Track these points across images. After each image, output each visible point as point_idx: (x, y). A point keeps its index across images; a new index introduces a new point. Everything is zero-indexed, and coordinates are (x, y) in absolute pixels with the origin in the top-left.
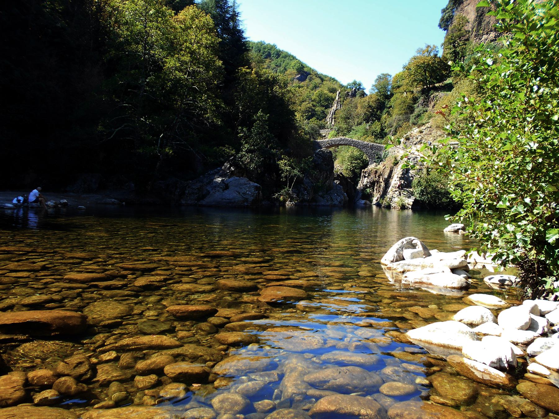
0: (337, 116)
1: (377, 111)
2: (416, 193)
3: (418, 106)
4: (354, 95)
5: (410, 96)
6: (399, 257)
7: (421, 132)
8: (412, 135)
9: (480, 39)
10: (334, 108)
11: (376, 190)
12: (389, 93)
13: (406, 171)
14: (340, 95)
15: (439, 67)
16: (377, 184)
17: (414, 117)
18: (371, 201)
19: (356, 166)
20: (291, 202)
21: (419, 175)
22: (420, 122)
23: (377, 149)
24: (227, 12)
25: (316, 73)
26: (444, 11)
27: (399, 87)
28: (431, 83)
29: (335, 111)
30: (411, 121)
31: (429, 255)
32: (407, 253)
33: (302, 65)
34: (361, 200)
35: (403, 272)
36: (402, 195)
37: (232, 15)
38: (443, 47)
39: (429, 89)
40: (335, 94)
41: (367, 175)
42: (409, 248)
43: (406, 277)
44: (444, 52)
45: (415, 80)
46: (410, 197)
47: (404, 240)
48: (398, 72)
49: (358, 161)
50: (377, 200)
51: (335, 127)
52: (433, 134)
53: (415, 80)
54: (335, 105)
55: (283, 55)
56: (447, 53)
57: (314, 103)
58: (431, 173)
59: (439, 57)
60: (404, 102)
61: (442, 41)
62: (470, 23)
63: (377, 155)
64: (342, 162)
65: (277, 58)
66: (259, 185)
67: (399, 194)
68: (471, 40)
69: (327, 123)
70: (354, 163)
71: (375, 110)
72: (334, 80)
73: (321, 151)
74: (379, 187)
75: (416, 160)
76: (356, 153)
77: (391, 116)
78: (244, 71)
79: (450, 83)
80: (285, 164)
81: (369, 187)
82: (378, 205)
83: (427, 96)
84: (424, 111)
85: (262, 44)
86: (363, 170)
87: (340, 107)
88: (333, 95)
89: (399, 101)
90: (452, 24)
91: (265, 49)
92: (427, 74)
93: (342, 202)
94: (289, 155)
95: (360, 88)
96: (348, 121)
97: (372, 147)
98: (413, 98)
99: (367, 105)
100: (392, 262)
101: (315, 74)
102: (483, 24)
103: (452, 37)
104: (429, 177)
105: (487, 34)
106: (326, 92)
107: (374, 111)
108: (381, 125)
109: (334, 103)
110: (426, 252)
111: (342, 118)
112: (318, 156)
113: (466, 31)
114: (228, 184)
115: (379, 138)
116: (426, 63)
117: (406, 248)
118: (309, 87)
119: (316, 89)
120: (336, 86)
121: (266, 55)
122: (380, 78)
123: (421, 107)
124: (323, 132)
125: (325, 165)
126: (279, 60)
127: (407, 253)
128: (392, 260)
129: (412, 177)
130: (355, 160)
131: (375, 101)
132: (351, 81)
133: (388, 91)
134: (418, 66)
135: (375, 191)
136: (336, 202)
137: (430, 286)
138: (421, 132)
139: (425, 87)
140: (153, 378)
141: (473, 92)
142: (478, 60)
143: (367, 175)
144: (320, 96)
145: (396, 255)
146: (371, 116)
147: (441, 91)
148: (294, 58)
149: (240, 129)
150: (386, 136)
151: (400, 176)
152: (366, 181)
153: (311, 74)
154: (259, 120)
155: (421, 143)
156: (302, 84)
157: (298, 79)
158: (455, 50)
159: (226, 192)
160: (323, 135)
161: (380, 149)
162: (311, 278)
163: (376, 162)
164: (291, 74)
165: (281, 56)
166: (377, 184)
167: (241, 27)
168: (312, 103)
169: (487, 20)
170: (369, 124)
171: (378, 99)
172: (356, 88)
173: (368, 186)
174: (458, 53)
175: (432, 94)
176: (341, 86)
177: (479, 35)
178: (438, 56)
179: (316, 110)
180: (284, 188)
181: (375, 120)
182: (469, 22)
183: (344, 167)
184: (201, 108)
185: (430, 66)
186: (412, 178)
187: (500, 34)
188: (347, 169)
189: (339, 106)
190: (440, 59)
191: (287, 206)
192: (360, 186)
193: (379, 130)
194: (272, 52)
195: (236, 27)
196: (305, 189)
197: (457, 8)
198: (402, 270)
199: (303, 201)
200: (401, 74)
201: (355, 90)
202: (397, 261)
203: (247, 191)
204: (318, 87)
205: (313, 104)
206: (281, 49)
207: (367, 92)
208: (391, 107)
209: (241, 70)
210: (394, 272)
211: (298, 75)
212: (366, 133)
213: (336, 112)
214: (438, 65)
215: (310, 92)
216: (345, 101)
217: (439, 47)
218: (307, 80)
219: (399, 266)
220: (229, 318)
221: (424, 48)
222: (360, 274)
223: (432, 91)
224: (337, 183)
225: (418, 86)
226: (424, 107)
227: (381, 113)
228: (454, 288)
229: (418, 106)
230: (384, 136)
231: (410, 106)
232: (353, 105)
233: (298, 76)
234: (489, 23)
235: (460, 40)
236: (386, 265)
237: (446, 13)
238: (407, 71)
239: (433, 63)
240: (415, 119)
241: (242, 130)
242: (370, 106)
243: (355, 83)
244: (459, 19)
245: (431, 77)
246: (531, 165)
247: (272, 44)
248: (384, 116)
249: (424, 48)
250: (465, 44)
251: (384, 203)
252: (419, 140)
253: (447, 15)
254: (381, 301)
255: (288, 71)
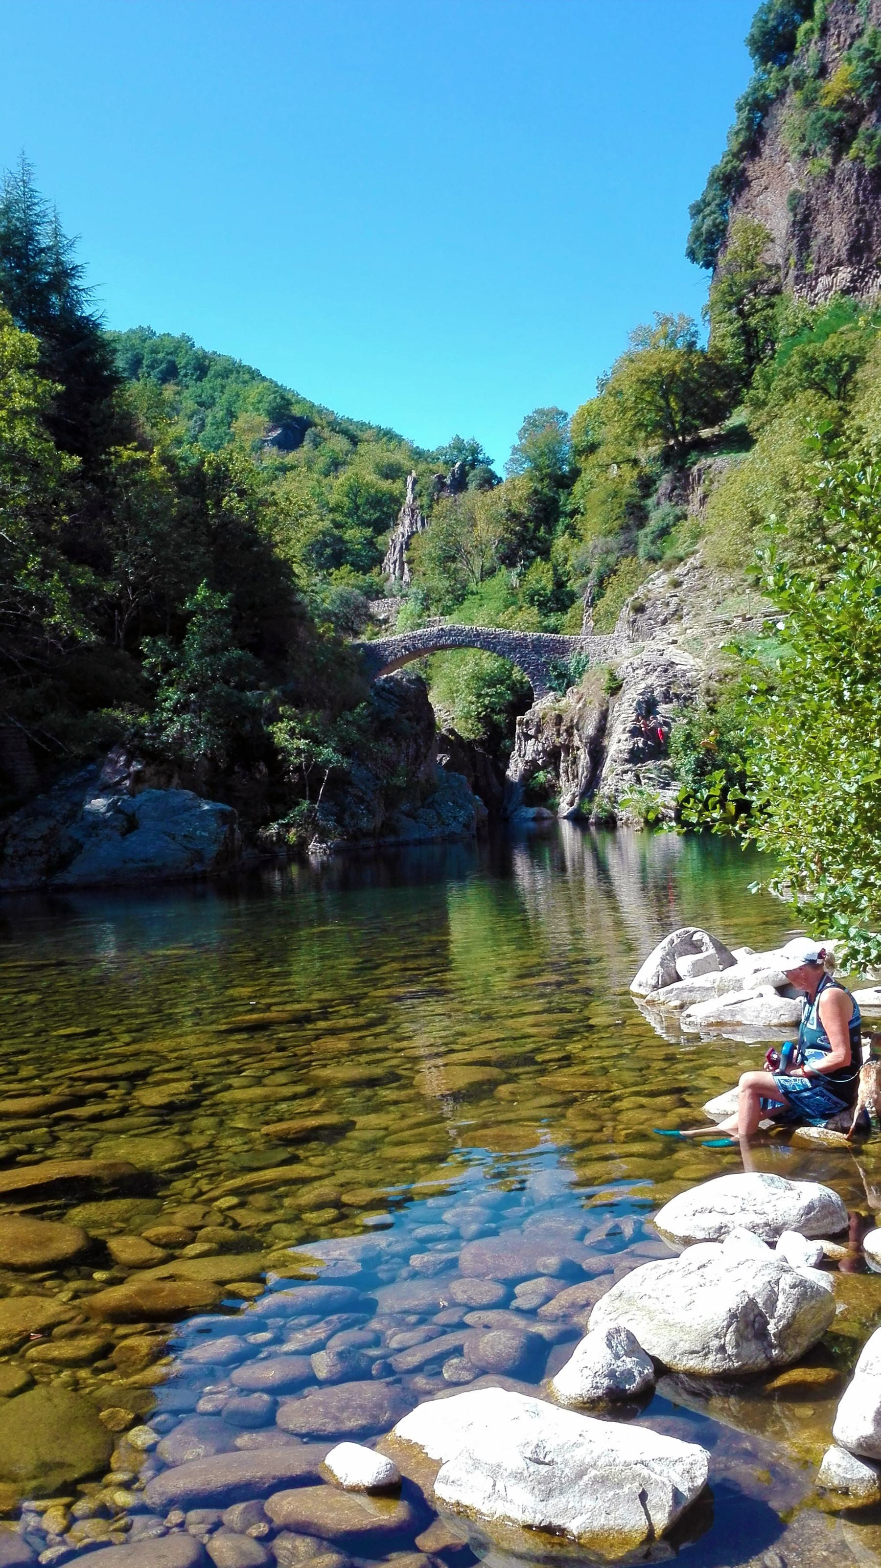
0: (416, 554)
1: (537, 529)
2: (683, 770)
3: (658, 504)
4: (460, 484)
5: (630, 474)
6: (669, 975)
7: (677, 584)
8: (650, 595)
9: (812, 288)
10: (403, 528)
11: (566, 772)
12: (566, 468)
13: (648, 707)
14: (418, 488)
15: (704, 380)
16: (567, 754)
17: (650, 538)
18: (554, 807)
19: (494, 703)
20: (321, 842)
21: (685, 716)
22: (669, 554)
23: (554, 650)
24: (38, 268)
25: (331, 418)
26: (697, 210)
27: (592, 448)
28: (687, 429)
29: (409, 537)
30: (641, 551)
31: (733, 962)
32: (684, 964)
33: (283, 398)
34: (524, 809)
35: (682, 1007)
36: (643, 781)
37: (54, 274)
38: (707, 318)
39: (685, 450)
40: (399, 484)
41: (532, 732)
42: (686, 953)
43: (689, 1016)
44: (714, 330)
45: (640, 426)
46: (669, 785)
47: (673, 935)
48: (584, 403)
49: (501, 688)
50: (571, 804)
51: (414, 589)
52: (711, 587)
53: (640, 426)
54: (407, 522)
55: (218, 368)
56: (724, 336)
57: (339, 518)
58: (719, 707)
59: (702, 351)
60: (615, 494)
61: (704, 298)
62: (778, 241)
63: (555, 668)
64: (452, 695)
65: (199, 379)
66: (228, 808)
67: (634, 779)
68: (787, 291)
69: (387, 579)
70: (487, 695)
71: (531, 525)
72: (388, 436)
73: (392, 678)
74: (575, 762)
75: (670, 674)
76: (490, 663)
77: (581, 540)
78: (129, 457)
79: (742, 427)
80: (292, 733)
81: (544, 767)
82: (579, 819)
83: (681, 469)
84: (678, 518)
85: (145, 334)
86: (518, 718)
87: (423, 525)
88: (395, 487)
89: (597, 494)
90: (726, 247)
91: (154, 351)
92: (673, 404)
93: (474, 825)
94: (297, 701)
95: (475, 460)
96: (453, 566)
97: (538, 646)
98: (640, 477)
99: (503, 511)
100: (656, 987)
101: (329, 424)
102: (816, 244)
103: (730, 285)
104: (716, 719)
105: (829, 272)
106: (371, 477)
107: (526, 528)
108: (555, 570)
109: (401, 514)
110: (724, 956)
111: (432, 559)
112: (384, 694)
113: (769, 267)
114: (134, 815)
115: (551, 610)
116: (665, 373)
117: (681, 955)
118: (316, 467)
119: (336, 469)
120: (399, 457)
121: (161, 372)
122: (532, 424)
123: (666, 506)
124: (378, 608)
125: (409, 719)
126: (208, 386)
127: (684, 964)
128: (654, 982)
129: (666, 724)
130: (489, 687)
131: (528, 499)
132: (445, 441)
133: (563, 461)
134: (644, 382)
135: (563, 777)
136: (455, 827)
137: (739, 1028)
138: (677, 584)
139: (672, 442)
140: (330, 1213)
141: (811, 454)
142: (813, 358)
143: (532, 732)
144: (354, 492)
145: (661, 971)
146: (519, 545)
147: (721, 453)
148: (254, 375)
149: (147, 645)
150: (573, 602)
151: (630, 726)
152: (530, 748)
153: (316, 425)
154: (203, 612)
155: (681, 617)
156: (291, 458)
157: (277, 442)
158: (744, 326)
159: (133, 837)
160: (382, 617)
161: (562, 648)
162: (497, 1044)
163: (554, 690)
164: (251, 430)
165: (211, 373)
166: (567, 754)
167: (87, 310)
168: (331, 516)
169: (824, 233)
170: (518, 569)
171: (536, 492)
172: (465, 461)
173: (540, 762)
174: (756, 331)
175: (694, 463)
176: (418, 455)
177: (806, 276)
178: (698, 347)
179: (346, 537)
180: (298, 804)
181: (534, 558)
182: (772, 241)
183: (458, 710)
184: (30, 600)
185: (679, 379)
186: (665, 729)
187: (864, 271)
188: (467, 716)
189: (419, 524)
190: (705, 357)
191: (312, 859)
192: (514, 770)
193: (550, 587)
194: (181, 361)
195: (71, 312)
196: (361, 800)
197: (734, 202)
198: (677, 1003)
199: (357, 835)
200: (595, 407)
201: (462, 467)
202: (665, 985)
203: (195, 830)
204: (344, 463)
205: (333, 521)
206: (209, 349)
207: (498, 469)
208: (575, 512)
209: (118, 455)
210: (662, 1008)
211: (273, 429)
212: (511, 600)
213: (413, 541)
214: (703, 374)
215: (319, 482)
216: (435, 506)
217: (698, 320)
218: (307, 445)
219: (669, 997)
220: (386, 1129)
221: (651, 322)
222: (591, 1022)
223: (693, 456)
224: (444, 762)
225: (650, 442)
226: (677, 504)
227: (550, 531)
228: (784, 1025)
229: (658, 504)
230: (568, 603)
231: (634, 506)
232: (461, 517)
233: (275, 434)
234: (829, 240)
235: (755, 295)
236: (644, 997)
237: (704, 218)
238: (612, 399)
239: (685, 371)
240: (653, 542)
241: (153, 646)
242: (514, 516)
243: (458, 446)
244: (745, 231)
245: (685, 411)
246: (853, 815)
247: (177, 334)
248: (561, 542)
249: (651, 322)
250: (772, 306)
251: (595, 811)
252: (672, 607)
253: (709, 222)
254: (648, 1067)
255: (241, 420)
